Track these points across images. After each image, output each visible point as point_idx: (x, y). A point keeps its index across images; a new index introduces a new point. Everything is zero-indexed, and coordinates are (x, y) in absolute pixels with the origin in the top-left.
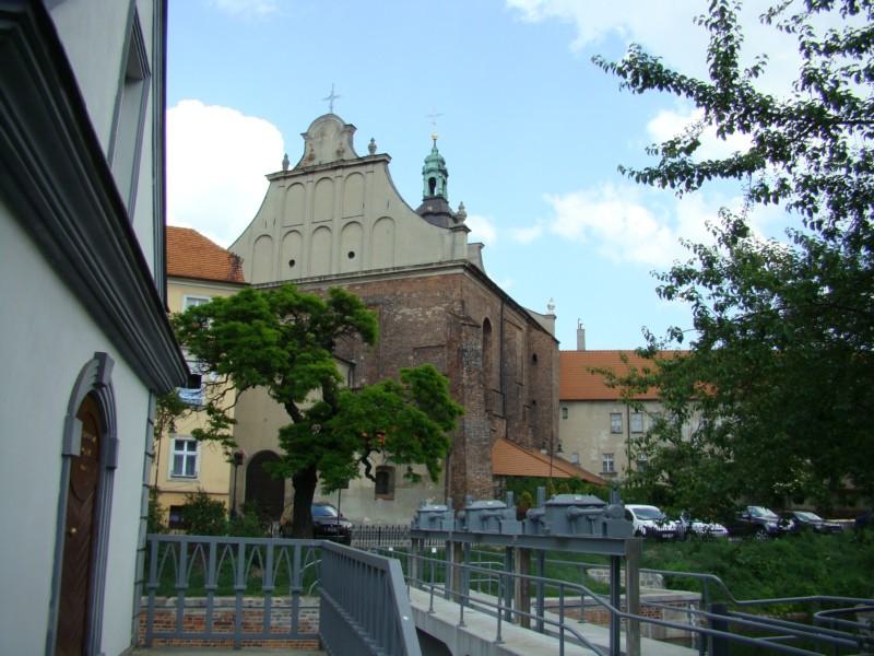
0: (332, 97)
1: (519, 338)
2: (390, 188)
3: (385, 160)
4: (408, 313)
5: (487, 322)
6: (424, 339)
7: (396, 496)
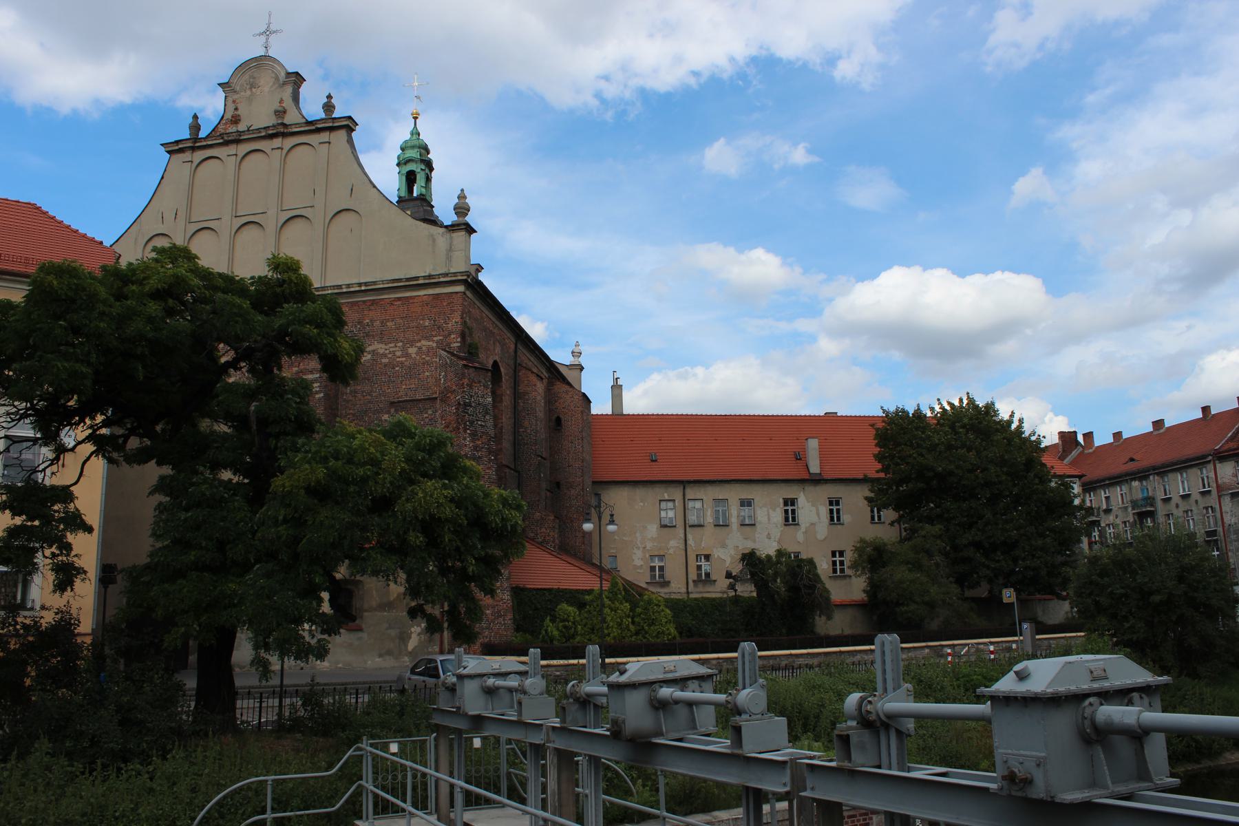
0: (268, 32)
1: (537, 390)
2: (356, 166)
3: (349, 125)
4: (381, 351)
5: (495, 364)
6: (405, 390)
7: (113, 563)
